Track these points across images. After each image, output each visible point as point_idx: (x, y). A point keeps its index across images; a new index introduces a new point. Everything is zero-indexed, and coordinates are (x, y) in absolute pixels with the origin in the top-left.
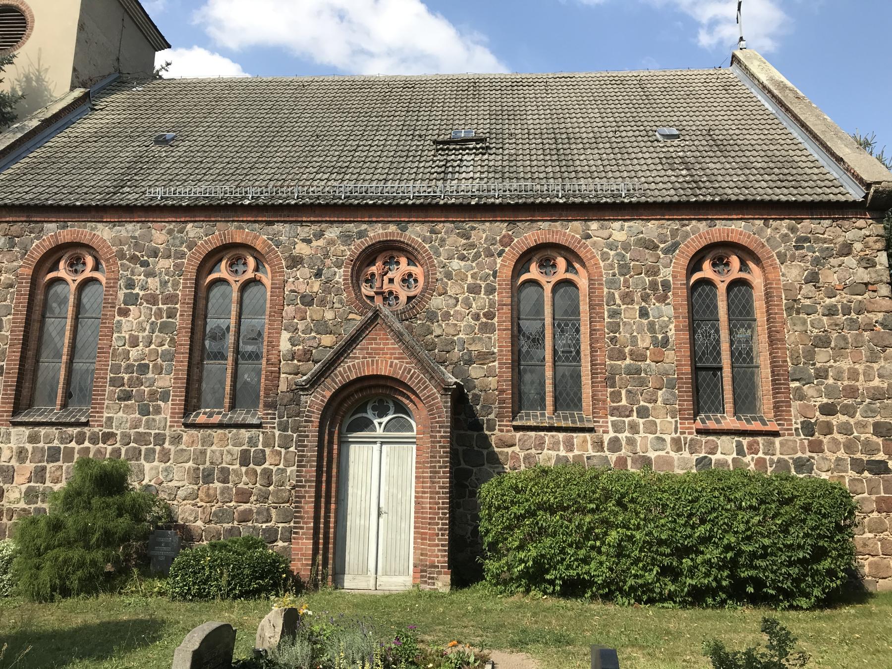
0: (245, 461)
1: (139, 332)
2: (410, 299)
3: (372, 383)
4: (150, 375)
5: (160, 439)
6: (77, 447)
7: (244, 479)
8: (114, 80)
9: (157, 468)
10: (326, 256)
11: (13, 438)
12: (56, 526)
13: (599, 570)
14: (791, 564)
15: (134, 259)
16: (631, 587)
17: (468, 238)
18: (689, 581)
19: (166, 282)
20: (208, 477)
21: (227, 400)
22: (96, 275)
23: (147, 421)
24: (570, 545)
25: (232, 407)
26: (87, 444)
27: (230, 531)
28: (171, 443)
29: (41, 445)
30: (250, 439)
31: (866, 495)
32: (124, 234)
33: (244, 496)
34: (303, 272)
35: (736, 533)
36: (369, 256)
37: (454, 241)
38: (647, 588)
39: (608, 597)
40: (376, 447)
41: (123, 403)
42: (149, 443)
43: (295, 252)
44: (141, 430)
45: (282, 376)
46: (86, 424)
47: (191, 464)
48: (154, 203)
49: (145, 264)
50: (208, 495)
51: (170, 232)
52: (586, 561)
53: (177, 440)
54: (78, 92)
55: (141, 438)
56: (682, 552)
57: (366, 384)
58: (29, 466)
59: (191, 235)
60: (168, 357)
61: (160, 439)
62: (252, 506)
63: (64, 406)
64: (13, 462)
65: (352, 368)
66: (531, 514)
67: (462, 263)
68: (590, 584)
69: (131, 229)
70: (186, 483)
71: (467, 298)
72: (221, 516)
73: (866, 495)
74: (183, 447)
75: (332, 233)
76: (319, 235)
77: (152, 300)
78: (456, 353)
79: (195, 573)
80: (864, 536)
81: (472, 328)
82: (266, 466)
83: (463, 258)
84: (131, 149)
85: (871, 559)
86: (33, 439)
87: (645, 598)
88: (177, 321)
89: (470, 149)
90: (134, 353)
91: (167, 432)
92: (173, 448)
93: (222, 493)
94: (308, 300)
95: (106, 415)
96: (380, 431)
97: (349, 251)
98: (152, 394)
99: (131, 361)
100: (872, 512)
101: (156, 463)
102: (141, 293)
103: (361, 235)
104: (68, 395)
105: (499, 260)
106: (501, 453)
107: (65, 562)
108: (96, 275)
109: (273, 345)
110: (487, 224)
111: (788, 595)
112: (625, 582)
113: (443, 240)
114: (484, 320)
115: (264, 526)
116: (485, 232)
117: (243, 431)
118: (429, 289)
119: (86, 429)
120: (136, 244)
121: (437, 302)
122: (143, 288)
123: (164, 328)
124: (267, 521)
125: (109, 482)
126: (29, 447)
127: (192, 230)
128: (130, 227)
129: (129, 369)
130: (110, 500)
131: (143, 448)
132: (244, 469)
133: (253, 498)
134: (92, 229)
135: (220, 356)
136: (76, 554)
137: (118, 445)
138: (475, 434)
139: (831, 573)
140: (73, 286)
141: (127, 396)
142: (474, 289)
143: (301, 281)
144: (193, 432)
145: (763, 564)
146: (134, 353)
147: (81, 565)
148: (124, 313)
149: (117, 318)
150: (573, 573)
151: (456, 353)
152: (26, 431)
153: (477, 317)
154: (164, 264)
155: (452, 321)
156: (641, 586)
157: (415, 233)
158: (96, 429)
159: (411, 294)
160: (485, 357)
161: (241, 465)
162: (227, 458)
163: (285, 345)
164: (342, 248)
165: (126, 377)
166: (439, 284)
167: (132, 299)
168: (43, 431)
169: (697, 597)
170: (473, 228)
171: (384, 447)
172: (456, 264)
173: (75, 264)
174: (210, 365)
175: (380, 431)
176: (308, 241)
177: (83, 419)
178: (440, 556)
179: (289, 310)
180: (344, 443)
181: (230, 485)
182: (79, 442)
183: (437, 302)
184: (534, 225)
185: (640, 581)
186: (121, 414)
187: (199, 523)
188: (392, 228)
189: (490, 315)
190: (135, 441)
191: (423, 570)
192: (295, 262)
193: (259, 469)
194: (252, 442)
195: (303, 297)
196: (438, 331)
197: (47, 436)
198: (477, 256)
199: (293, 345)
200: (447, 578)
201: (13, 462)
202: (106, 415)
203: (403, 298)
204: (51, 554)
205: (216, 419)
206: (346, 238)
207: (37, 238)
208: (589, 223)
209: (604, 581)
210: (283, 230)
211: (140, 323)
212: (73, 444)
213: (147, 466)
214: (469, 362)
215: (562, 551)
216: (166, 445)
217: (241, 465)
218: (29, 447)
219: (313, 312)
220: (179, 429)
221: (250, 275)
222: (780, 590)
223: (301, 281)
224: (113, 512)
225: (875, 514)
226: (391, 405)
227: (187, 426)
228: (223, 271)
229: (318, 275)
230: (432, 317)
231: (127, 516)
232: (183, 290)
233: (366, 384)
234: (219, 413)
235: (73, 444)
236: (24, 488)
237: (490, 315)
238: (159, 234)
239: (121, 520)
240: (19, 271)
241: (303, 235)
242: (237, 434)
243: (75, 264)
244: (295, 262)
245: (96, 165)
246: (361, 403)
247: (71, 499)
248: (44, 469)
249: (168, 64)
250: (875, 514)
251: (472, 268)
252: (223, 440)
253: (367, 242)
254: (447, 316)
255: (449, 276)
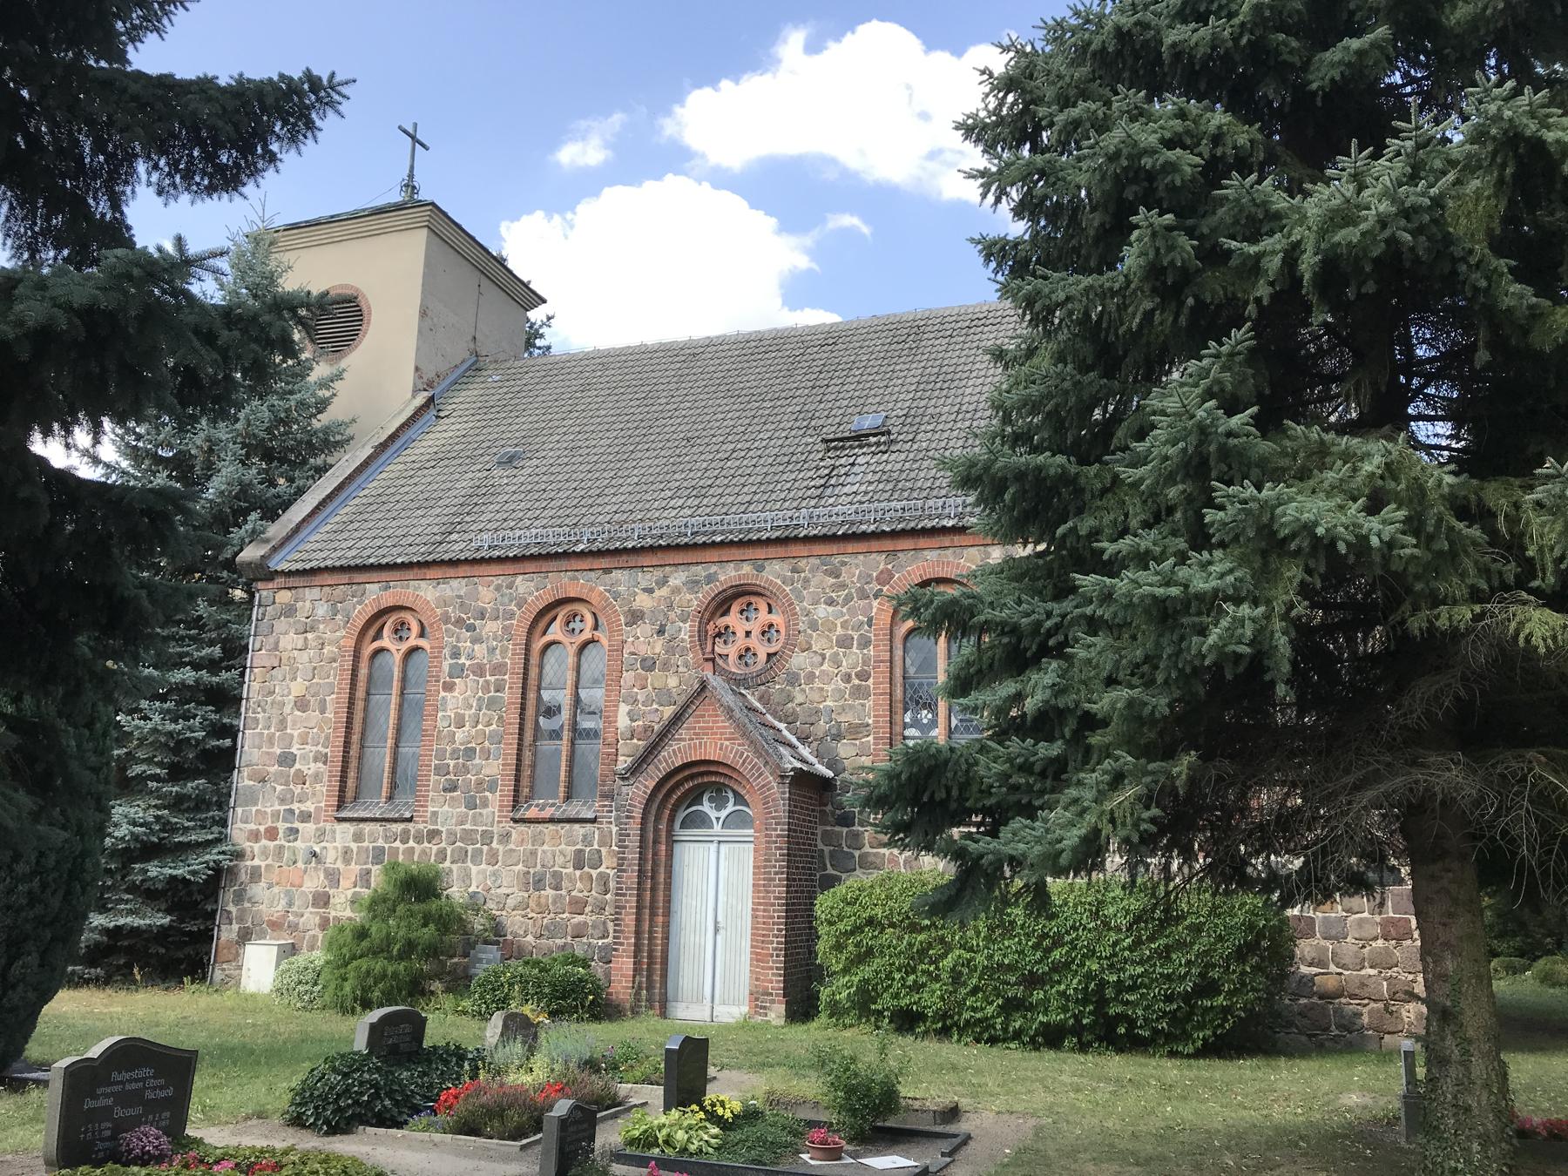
0: (579, 866)
1: (466, 712)
2: (769, 656)
3: (702, 769)
4: (477, 761)
5: (487, 837)
6: (402, 847)
7: (579, 885)
8: (469, 369)
9: (484, 871)
10: (670, 607)
11: (338, 836)
12: (362, 934)
13: (931, 999)
14: (1169, 999)
15: (459, 622)
16: (967, 1022)
17: (837, 577)
18: (1041, 1018)
19: (494, 649)
20: (539, 884)
21: (562, 789)
22: (422, 643)
23: (474, 816)
24: (899, 970)
25: (568, 797)
26: (411, 843)
27: (563, 947)
28: (500, 842)
29: (365, 844)
30: (585, 836)
31: (1366, 915)
32: (449, 593)
33: (578, 906)
34: (644, 630)
35: (1100, 958)
36: (723, 604)
37: (821, 581)
38: (985, 1023)
39: (944, 1033)
40: (713, 847)
41: (449, 795)
42: (473, 844)
43: (635, 606)
44: (467, 827)
45: (621, 758)
46: (410, 820)
47: (520, 866)
48: (478, 555)
49: (471, 628)
50: (539, 904)
51: (498, 588)
52: (917, 987)
53: (505, 837)
54: (420, 399)
55: (468, 837)
56: (1033, 981)
57: (695, 770)
58: (355, 868)
59: (521, 590)
60: (497, 739)
61: (487, 837)
62: (588, 918)
63: (390, 798)
64: (339, 865)
65: (675, 753)
66: (857, 930)
67: (830, 609)
68: (920, 1017)
69: (456, 587)
70: (515, 889)
71: (837, 654)
72: (553, 930)
73: (1366, 915)
74: (512, 846)
75: (678, 578)
76: (663, 582)
77: (479, 671)
78: (822, 726)
79: (494, 990)
80: (1363, 972)
81: (841, 692)
82: (602, 869)
83: (831, 602)
84: (470, 475)
85: (1373, 1005)
86: (358, 837)
87: (986, 1036)
88: (505, 695)
89: (869, 445)
90: (460, 735)
91: (495, 829)
92: (501, 848)
93: (554, 902)
94: (649, 664)
95: (430, 809)
96: (717, 828)
97: (695, 601)
98: (480, 783)
99: (457, 745)
100: (1376, 939)
101: (483, 866)
102: (468, 663)
103: (710, 579)
104: (393, 786)
105: (875, 603)
106: (875, 855)
107: (368, 973)
108: (422, 643)
109: (611, 722)
110: (861, 557)
111: (1169, 1037)
112: (960, 1014)
113: (806, 580)
114: (857, 682)
115: (600, 942)
116: (860, 565)
117: (577, 826)
118: (790, 645)
119: (410, 826)
120: (462, 604)
121: (799, 661)
122: (470, 657)
123: (492, 704)
124: (603, 937)
125: (418, 888)
126: (354, 846)
127: (523, 585)
128: (455, 583)
129: (455, 754)
130: (416, 907)
131: (470, 848)
132: (578, 873)
133: (588, 909)
134: (416, 589)
135: (555, 735)
136: (378, 965)
137: (443, 845)
138: (845, 830)
139: (1226, 1011)
140: (398, 657)
141: (453, 788)
142: (845, 643)
143: (642, 641)
144: (522, 827)
145: (1132, 998)
146: (460, 735)
147: (384, 976)
148: (449, 687)
149: (442, 694)
150: (903, 1003)
151: (822, 726)
152: (350, 828)
153: (847, 678)
154: (491, 627)
155: (817, 684)
156: (980, 1021)
157: (774, 572)
158: (421, 826)
159: (772, 650)
160: (857, 730)
161: (575, 868)
162: (560, 860)
163: (623, 721)
164: (688, 596)
165: (452, 763)
166: (801, 638)
167: (457, 671)
168: (367, 828)
169: (1052, 1038)
170: (844, 564)
171: (723, 846)
172: (822, 611)
173: (400, 630)
174: (546, 746)
175: (717, 828)
176: (650, 591)
177: (407, 815)
178: (775, 983)
179: (628, 677)
180: (671, 842)
181: (563, 892)
182: (404, 841)
183: (799, 661)
184: (920, 554)
185: (978, 1015)
186: (446, 808)
187: (530, 938)
188: (747, 568)
189: (864, 676)
190: (462, 840)
191: (758, 998)
192: (635, 617)
193: (594, 873)
194: (587, 840)
195: (644, 660)
196: (799, 698)
197: (371, 834)
198: (848, 599)
199: (632, 720)
200: (781, 1008)
201: (339, 865)
202: (430, 809)
203: (762, 657)
204: (355, 963)
205: (547, 813)
206: (693, 584)
207: (359, 603)
208: (989, 549)
209: (936, 1013)
210: (621, 578)
211: (466, 699)
212: (397, 844)
213: (474, 869)
214: (838, 737)
215: (889, 976)
216: (494, 845)
217: (575, 868)
218: (354, 846)
219: (655, 678)
220: (509, 825)
221: (587, 635)
222: (1155, 1031)
223: (642, 641)
224: (416, 922)
225: (1380, 943)
226: (730, 795)
227: (515, 821)
228: (556, 631)
229: (661, 632)
230: (793, 680)
231: (432, 926)
232: (512, 659)
233: (695, 770)
234: (553, 805)
235: (397, 844)
236: (349, 893)
237: (864, 676)
238: (486, 590)
239: (425, 930)
240: (342, 642)
241: (644, 584)
242: (571, 830)
243: (400, 630)
244: (635, 617)
245: (427, 504)
246: (686, 791)
247: (378, 906)
248: (369, 872)
249: (549, 318)
250: (1380, 943)
251: (843, 615)
252: (556, 837)
253: (716, 588)
254: (811, 677)
255: (814, 626)
